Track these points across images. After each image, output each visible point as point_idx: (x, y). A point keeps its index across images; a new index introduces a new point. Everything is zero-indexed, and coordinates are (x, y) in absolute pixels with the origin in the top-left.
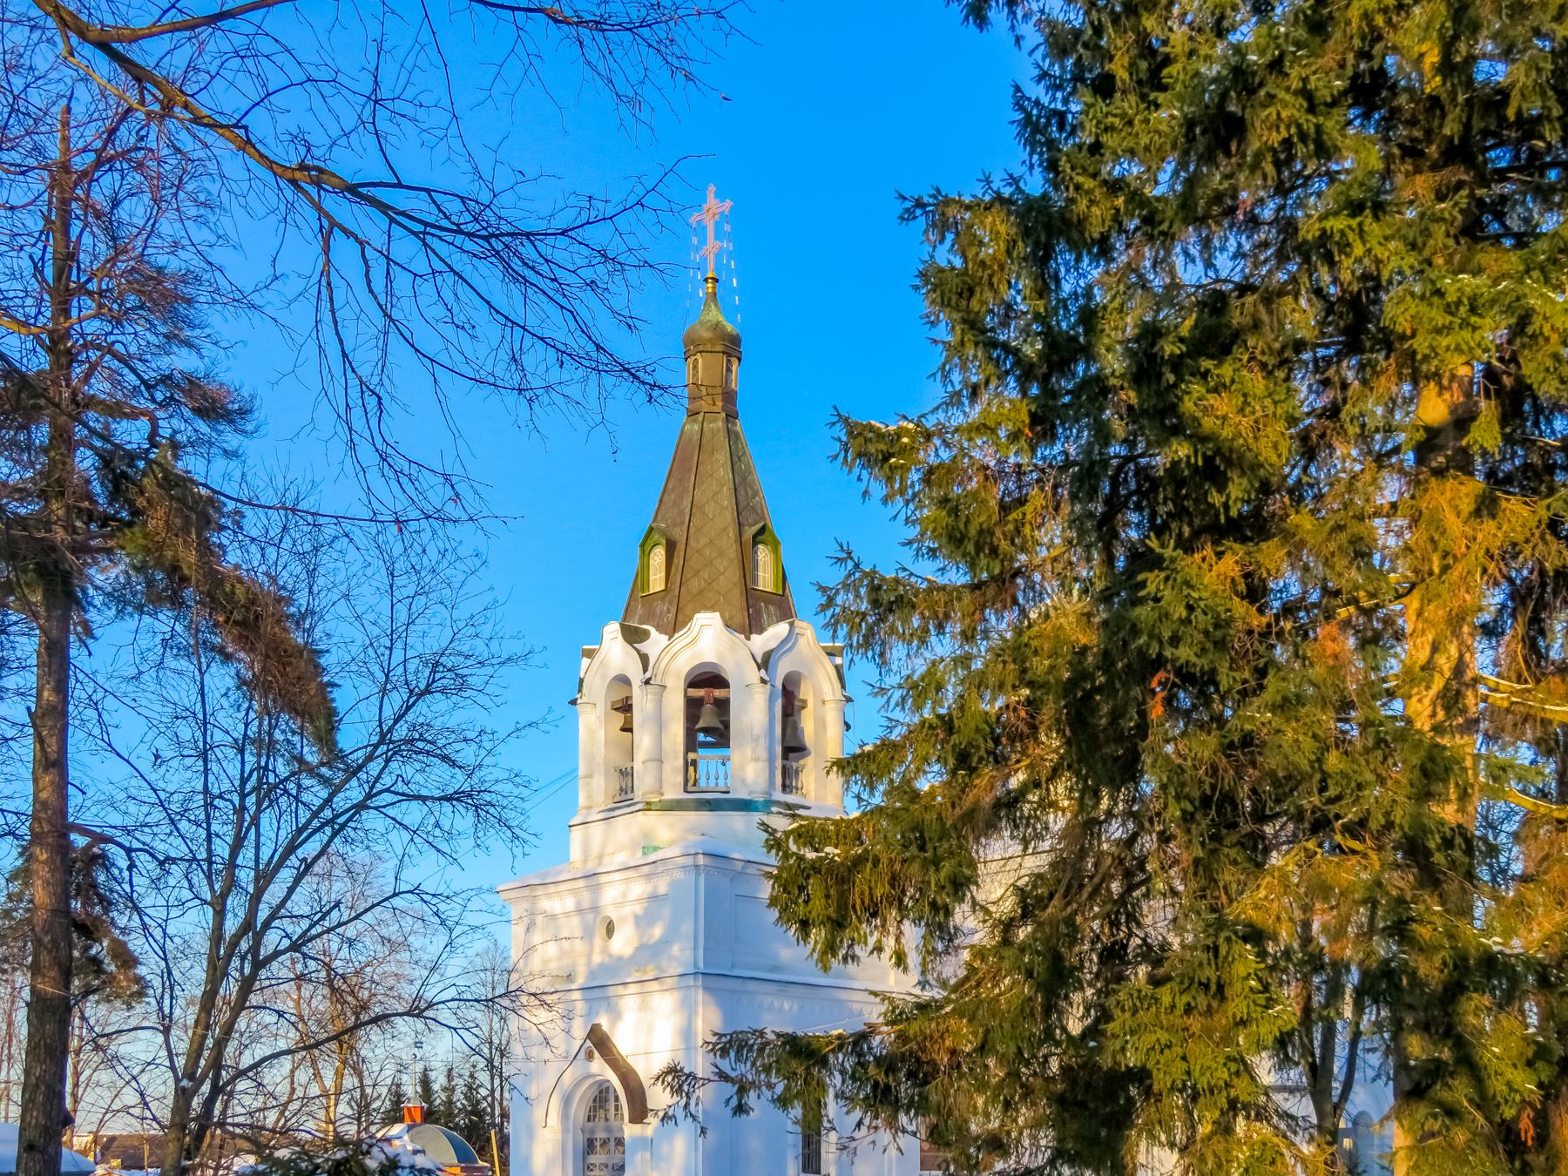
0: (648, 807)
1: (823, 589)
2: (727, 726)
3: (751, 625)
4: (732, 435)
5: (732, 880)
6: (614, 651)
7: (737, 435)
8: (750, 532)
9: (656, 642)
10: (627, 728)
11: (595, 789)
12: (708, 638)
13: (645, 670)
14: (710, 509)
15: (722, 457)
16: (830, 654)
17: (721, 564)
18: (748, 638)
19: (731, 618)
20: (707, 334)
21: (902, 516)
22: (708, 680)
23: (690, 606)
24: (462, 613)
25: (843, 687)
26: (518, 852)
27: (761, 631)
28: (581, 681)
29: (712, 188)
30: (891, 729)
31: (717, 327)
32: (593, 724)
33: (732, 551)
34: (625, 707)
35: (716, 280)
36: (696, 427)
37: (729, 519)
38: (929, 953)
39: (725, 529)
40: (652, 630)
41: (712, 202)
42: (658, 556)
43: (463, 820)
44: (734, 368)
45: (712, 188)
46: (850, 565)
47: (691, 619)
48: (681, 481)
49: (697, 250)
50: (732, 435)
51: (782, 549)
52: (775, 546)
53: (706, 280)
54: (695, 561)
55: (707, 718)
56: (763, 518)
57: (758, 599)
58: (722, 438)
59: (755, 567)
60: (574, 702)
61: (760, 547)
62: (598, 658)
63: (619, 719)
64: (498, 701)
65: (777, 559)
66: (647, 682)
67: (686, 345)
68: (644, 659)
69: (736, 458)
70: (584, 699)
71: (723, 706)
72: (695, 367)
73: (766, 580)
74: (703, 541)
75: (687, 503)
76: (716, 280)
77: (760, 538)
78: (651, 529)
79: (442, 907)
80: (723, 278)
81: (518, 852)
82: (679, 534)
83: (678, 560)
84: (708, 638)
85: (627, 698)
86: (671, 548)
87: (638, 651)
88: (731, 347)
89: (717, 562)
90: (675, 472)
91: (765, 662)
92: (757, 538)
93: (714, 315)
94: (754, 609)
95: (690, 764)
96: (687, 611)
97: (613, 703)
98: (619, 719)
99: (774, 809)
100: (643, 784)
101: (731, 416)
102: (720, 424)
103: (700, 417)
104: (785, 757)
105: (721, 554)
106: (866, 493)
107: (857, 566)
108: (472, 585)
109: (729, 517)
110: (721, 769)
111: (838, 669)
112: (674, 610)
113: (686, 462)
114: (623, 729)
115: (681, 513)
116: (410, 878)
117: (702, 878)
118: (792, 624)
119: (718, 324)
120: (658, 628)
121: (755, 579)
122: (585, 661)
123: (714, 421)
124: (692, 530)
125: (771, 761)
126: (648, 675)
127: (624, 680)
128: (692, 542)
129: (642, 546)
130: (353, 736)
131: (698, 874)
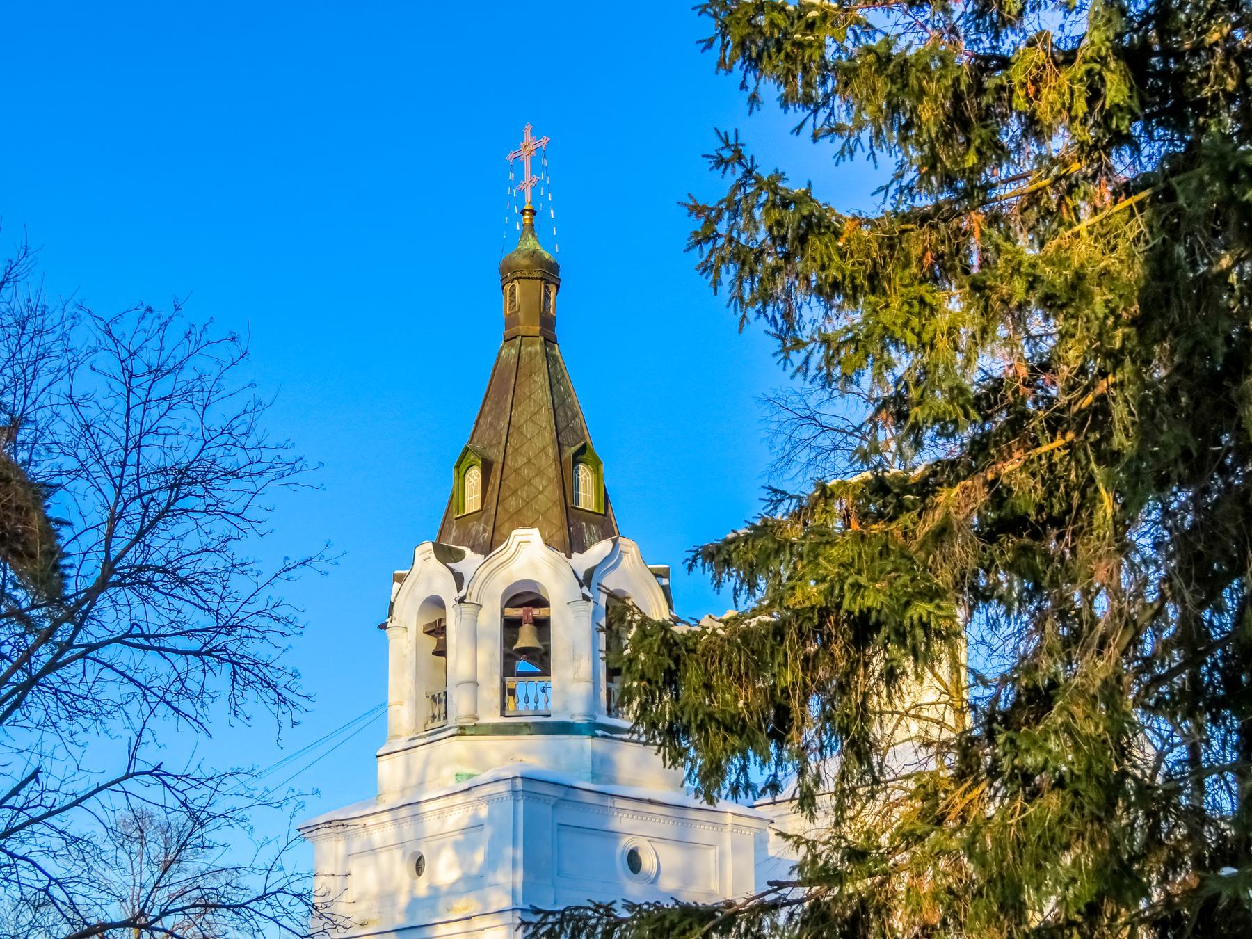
0: (462, 731)
1: (696, 210)
2: (547, 653)
3: (573, 544)
4: (550, 359)
5: (554, 807)
6: (428, 573)
7: (555, 359)
8: (569, 452)
9: (471, 561)
10: (441, 652)
11: (403, 713)
12: (528, 555)
13: (459, 589)
14: (528, 429)
15: (541, 379)
16: (656, 576)
17: (539, 483)
18: (569, 557)
19: (551, 536)
20: (526, 262)
21: (808, 129)
22: (526, 602)
23: (507, 525)
24: (215, 419)
25: (671, 607)
26: (286, 720)
27: (583, 549)
28: (392, 604)
29: (529, 127)
30: (776, 504)
31: (534, 254)
32: (405, 639)
33: (552, 471)
34: (437, 630)
35: (533, 212)
36: (513, 351)
37: (548, 440)
38: (844, 795)
39: (544, 448)
40: (468, 551)
41: (529, 139)
42: (474, 478)
43: (219, 680)
44: (552, 295)
45: (529, 127)
46: (740, 171)
47: (507, 536)
48: (497, 403)
49: (513, 184)
50: (550, 359)
51: (603, 468)
52: (596, 465)
53: (523, 212)
54: (512, 481)
55: (526, 638)
56: (584, 438)
57: (579, 518)
58: (540, 361)
59: (577, 487)
60: (383, 627)
61: (581, 466)
62: (408, 583)
63: (432, 643)
64: (262, 528)
65: (599, 479)
66: (461, 601)
67: (502, 273)
68: (459, 579)
69: (555, 381)
70: (395, 623)
71: (542, 626)
72: (512, 294)
73: (587, 499)
74: (521, 460)
75: (504, 423)
76: (533, 212)
77: (581, 457)
78: (467, 450)
79: (191, 794)
80: (540, 208)
81: (286, 720)
82: (495, 455)
83: (495, 480)
84: (528, 555)
85: (440, 620)
86: (487, 468)
87: (452, 570)
88: (549, 273)
89: (536, 481)
90: (492, 395)
91: (587, 579)
92: (577, 459)
93: (531, 243)
94: (573, 531)
95: (507, 692)
96: (504, 531)
97: (426, 627)
98: (432, 643)
99: (599, 732)
100: (460, 705)
101: (550, 341)
102: (538, 347)
103: (518, 341)
104: (610, 679)
105: (540, 473)
106: (754, 99)
107: (748, 172)
108: (232, 381)
109: (548, 437)
110: (542, 697)
111: (665, 589)
112: (490, 529)
113: (503, 385)
114: (436, 653)
115: (498, 434)
116: (148, 756)
117: (521, 804)
118: (615, 542)
119: (535, 252)
120: (473, 548)
121: (576, 498)
122: (396, 585)
123: (532, 344)
124: (510, 450)
125: (595, 681)
126: (462, 593)
127: (436, 603)
128: (509, 462)
129: (458, 467)
130: (82, 573)
131: (516, 801)
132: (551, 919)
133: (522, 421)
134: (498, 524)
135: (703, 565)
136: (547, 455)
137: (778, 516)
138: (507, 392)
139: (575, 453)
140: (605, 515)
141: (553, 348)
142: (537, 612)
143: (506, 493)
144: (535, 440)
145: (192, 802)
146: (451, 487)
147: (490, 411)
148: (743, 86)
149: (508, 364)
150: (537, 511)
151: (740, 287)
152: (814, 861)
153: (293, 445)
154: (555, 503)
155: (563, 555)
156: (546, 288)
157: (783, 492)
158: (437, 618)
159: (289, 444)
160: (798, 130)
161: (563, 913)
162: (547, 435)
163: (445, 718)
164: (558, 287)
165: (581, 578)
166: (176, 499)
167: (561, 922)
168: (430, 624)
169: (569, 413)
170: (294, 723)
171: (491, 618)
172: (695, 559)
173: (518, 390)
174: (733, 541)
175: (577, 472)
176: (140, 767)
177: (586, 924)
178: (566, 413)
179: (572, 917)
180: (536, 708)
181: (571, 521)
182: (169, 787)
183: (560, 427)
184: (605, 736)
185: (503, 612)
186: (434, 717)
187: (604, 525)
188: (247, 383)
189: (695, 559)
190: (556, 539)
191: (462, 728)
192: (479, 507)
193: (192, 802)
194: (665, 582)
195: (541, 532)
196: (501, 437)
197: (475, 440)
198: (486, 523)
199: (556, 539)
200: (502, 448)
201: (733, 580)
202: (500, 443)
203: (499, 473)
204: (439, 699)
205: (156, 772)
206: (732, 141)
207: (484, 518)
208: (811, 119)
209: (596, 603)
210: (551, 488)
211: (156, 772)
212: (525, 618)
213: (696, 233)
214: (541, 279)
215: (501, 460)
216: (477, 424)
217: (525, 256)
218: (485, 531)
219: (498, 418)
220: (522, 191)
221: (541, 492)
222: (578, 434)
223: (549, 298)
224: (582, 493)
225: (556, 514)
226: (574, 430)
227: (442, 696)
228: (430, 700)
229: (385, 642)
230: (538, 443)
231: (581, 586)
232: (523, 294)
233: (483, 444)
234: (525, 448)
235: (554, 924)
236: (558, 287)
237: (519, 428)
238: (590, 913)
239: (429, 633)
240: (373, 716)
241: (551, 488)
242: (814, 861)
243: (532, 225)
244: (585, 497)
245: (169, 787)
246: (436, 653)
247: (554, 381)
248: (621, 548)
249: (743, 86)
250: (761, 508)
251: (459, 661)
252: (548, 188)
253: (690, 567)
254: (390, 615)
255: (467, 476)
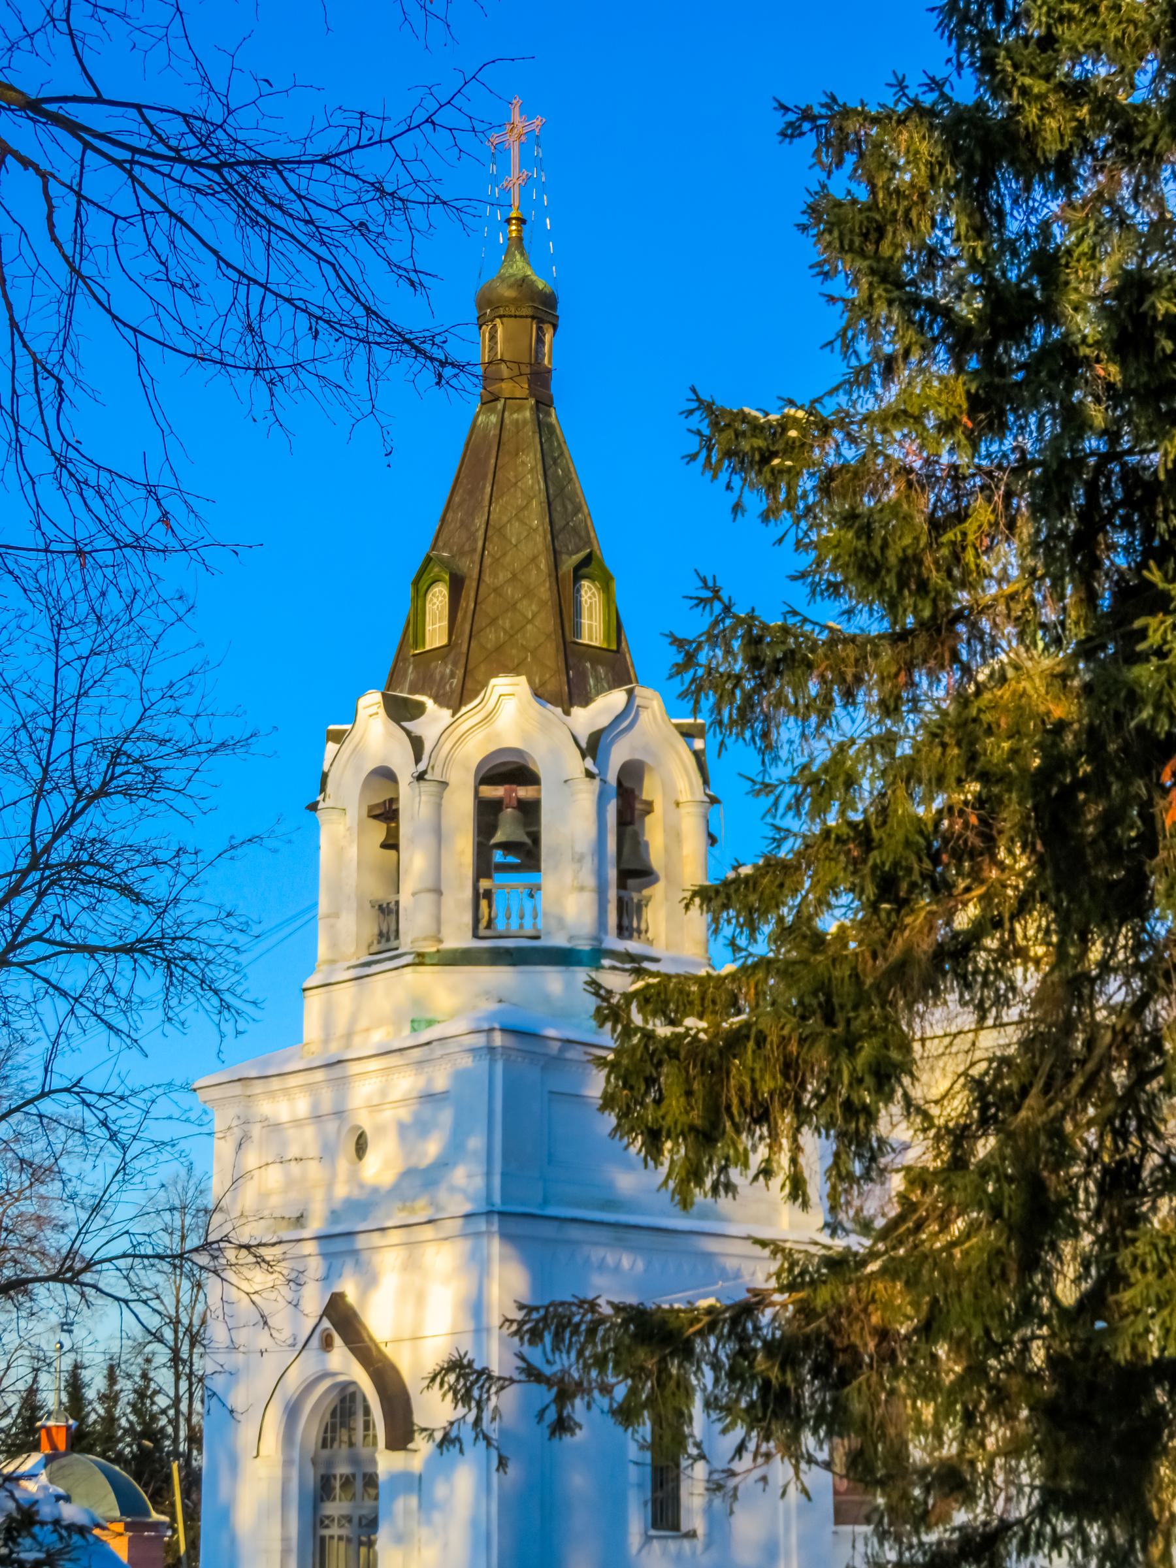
0: (421, 960)
1: (679, 643)
3: (572, 695)
4: (544, 429)
5: (543, 1068)
6: (373, 731)
9: (434, 719)
10: (391, 843)
11: (341, 931)
12: (508, 711)
13: (418, 760)
14: (514, 531)
15: (530, 459)
17: (529, 608)
18: (567, 713)
19: (543, 684)
20: (509, 293)
21: (790, 540)
23: (483, 668)
24: (156, 680)
25: (706, 782)
26: (228, 1028)
27: (586, 702)
28: (325, 776)
30: (779, 842)
31: (523, 283)
32: (341, 836)
33: (544, 591)
35: (522, 221)
36: (494, 419)
37: (541, 546)
38: (838, 1173)
40: (429, 703)
42: (438, 598)
44: (547, 338)
46: (718, 607)
47: (485, 685)
48: (471, 493)
51: (616, 586)
52: (606, 582)
53: (508, 221)
54: (490, 606)
56: (588, 542)
58: (529, 431)
60: (313, 807)
61: (585, 583)
66: (421, 777)
68: (417, 744)
70: (329, 803)
71: (530, 811)
72: (493, 337)
73: (593, 630)
74: (503, 576)
75: (480, 522)
76: (522, 221)
77: (584, 571)
78: (428, 560)
79: (113, 1113)
80: (532, 216)
82: (468, 566)
83: (467, 604)
84: (508, 711)
86: (456, 586)
87: (408, 733)
88: (543, 309)
89: (523, 605)
92: (579, 573)
93: (519, 267)
94: (570, 675)
95: (481, 897)
96: (479, 676)
97: (371, 808)
98: (379, 831)
100: (414, 928)
101: (543, 403)
102: (528, 414)
103: (500, 405)
104: (622, 885)
105: (529, 593)
107: (727, 609)
109: (539, 543)
110: (528, 904)
112: (460, 673)
114: (385, 846)
115: (472, 537)
117: (499, 1067)
118: (630, 693)
120: (437, 700)
121: (577, 630)
122: (331, 747)
123: (519, 409)
124: (488, 561)
125: (601, 891)
126: (422, 766)
127: (386, 775)
128: (487, 578)
129: (416, 583)
131: (492, 1061)
132: (535, 1316)
133: (505, 519)
134: (470, 667)
135: (701, 906)
136: (538, 568)
137: (782, 855)
138: (484, 478)
139: (576, 561)
140: (618, 651)
141: (548, 414)
142: (523, 792)
143: (481, 622)
144: (522, 547)
145: (114, 1122)
146: (406, 607)
147: (460, 504)
148: (729, 487)
149: (485, 437)
150: (524, 648)
151: (719, 713)
152: (791, 1270)
153: (245, 712)
154: (548, 636)
155: (559, 710)
156: (540, 329)
157: (788, 830)
158: (388, 797)
159: (240, 711)
160: (780, 541)
161: (547, 1308)
162: (539, 539)
163: (397, 936)
164: (555, 327)
165: (584, 745)
166: (112, 778)
167: (544, 1318)
168: (377, 805)
169: (570, 507)
170: (238, 1033)
171: (461, 805)
172: (692, 899)
173: (499, 475)
174: (734, 881)
175: (579, 591)
176: (57, 1082)
177: (570, 1320)
178: (564, 506)
179: (556, 1315)
180: (521, 926)
181: (571, 661)
182: (88, 1105)
183: (557, 527)
184: (614, 968)
185: (476, 792)
186: (381, 934)
187: (616, 667)
188: (193, 644)
189: (692, 899)
190: (549, 687)
191: (420, 954)
192: (445, 641)
193: (114, 1122)
194: (699, 744)
195: (530, 681)
196: (475, 541)
197: (440, 544)
198: (455, 664)
199: (549, 687)
200: (477, 557)
201: (732, 927)
202: (474, 550)
203: (472, 594)
204: (388, 912)
205: (75, 1089)
206: (710, 584)
207: (451, 657)
208: (793, 530)
209: (604, 781)
210: (543, 615)
211: (75, 1089)
212: (506, 801)
213: (677, 665)
214: (533, 317)
215: (475, 575)
216: (443, 520)
217: (510, 286)
218: (452, 675)
219: (471, 515)
220: (506, 191)
221: (529, 621)
222: (583, 537)
223: (543, 343)
224: (585, 621)
225: (550, 653)
226: (575, 530)
227: (392, 906)
228: (375, 912)
229: (317, 828)
230: (527, 550)
231: (584, 757)
232: (507, 340)
233: (450, 551)
234: (508, 558)
235: (537, 1321)
236: (555, 327)
237: (500, 530)
238: (574, 1309)
239: (376, 817)
240: (299, 922)
241: (543, 615)
242: (791, 1270)
243: (520, 239)
244: (590, 626)
245: (88, 1105)
246: (385, 846)
247: (549, 461)
248: (638, 701)
249: (729, 487)
250: (765, 847)
251: (415, 861)
252: (543, 188)
253: (687, 907)
254: (323, 789)
255: (429, 596)
